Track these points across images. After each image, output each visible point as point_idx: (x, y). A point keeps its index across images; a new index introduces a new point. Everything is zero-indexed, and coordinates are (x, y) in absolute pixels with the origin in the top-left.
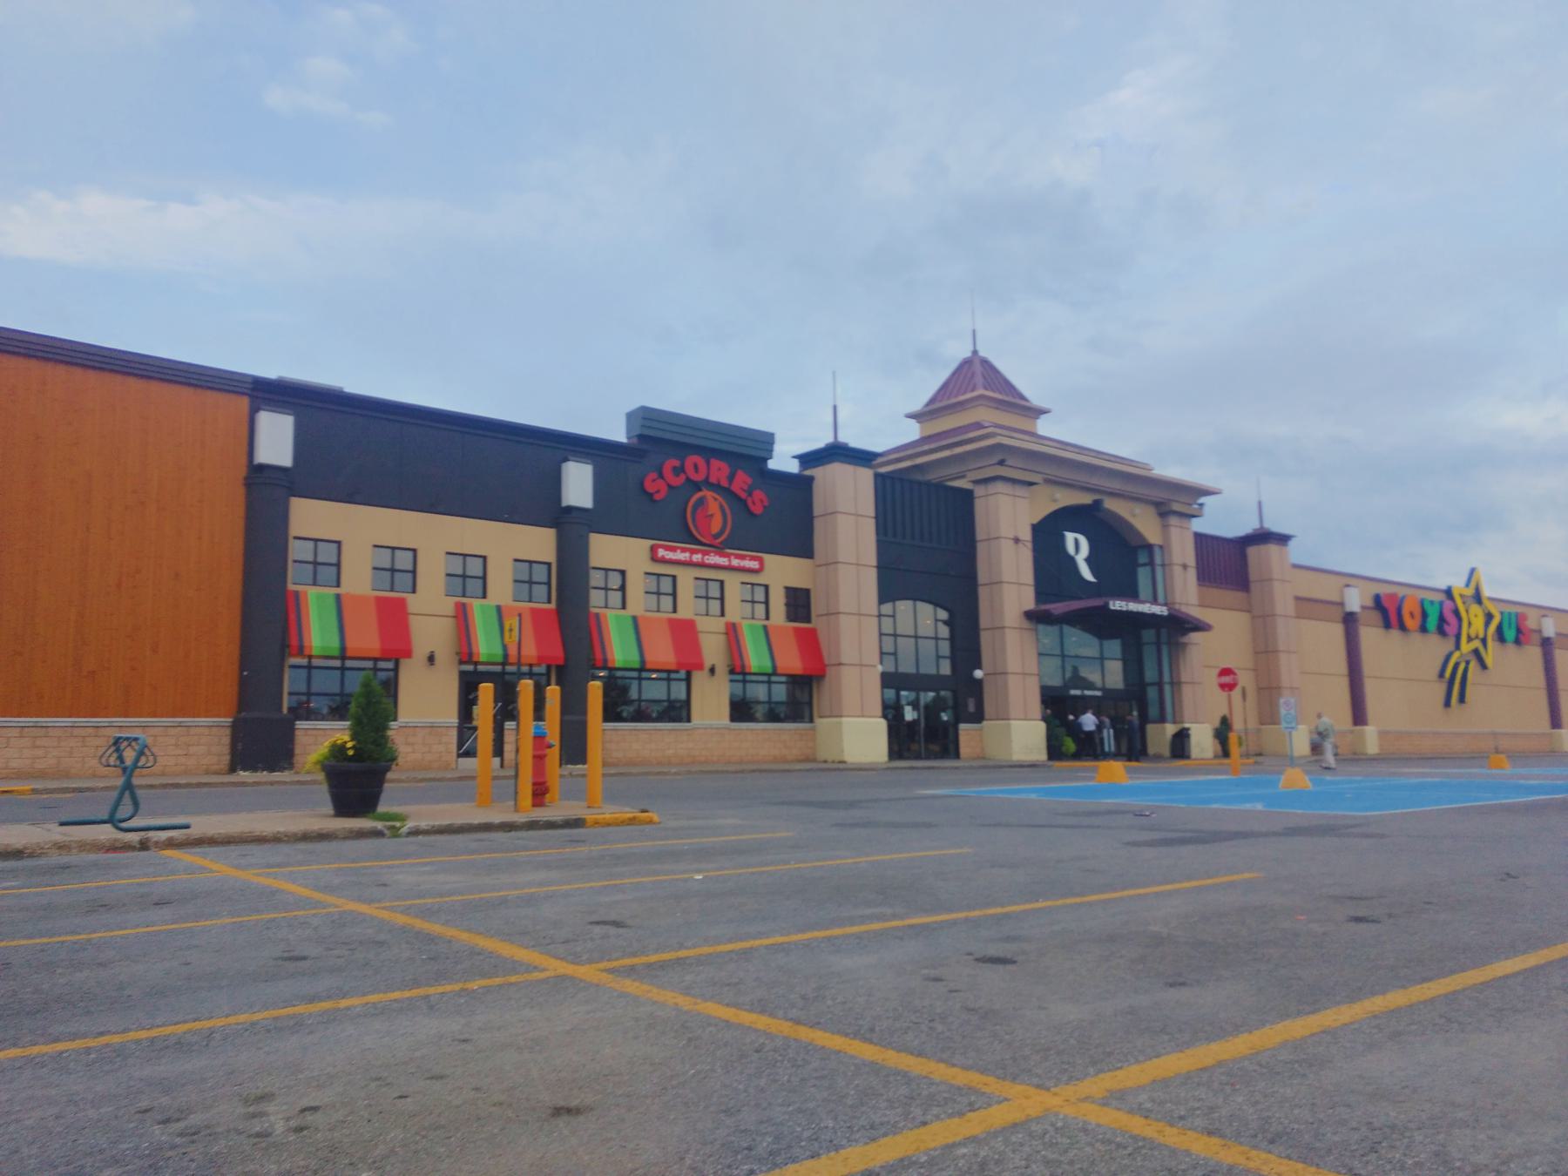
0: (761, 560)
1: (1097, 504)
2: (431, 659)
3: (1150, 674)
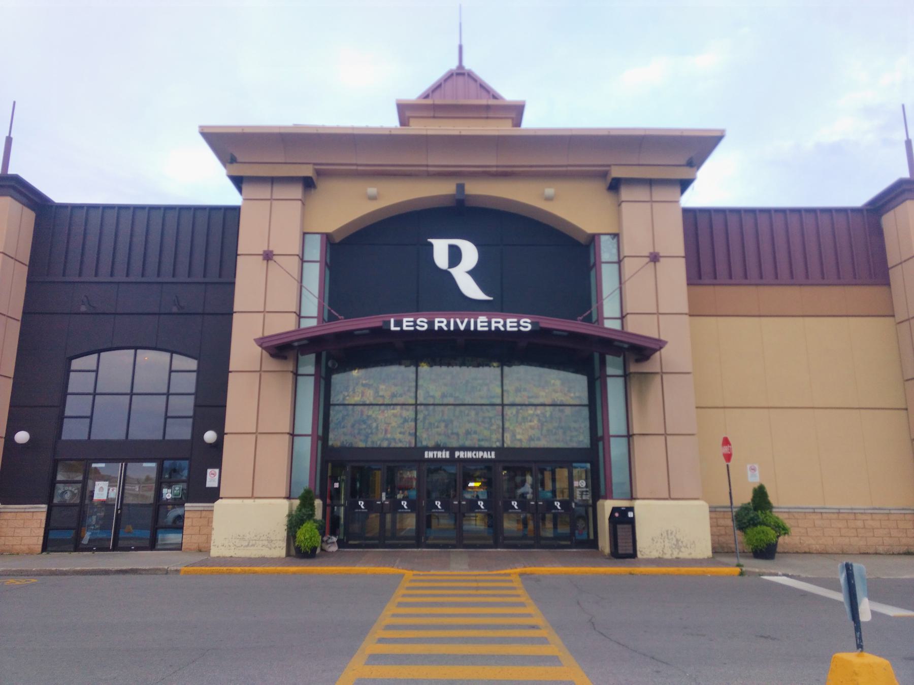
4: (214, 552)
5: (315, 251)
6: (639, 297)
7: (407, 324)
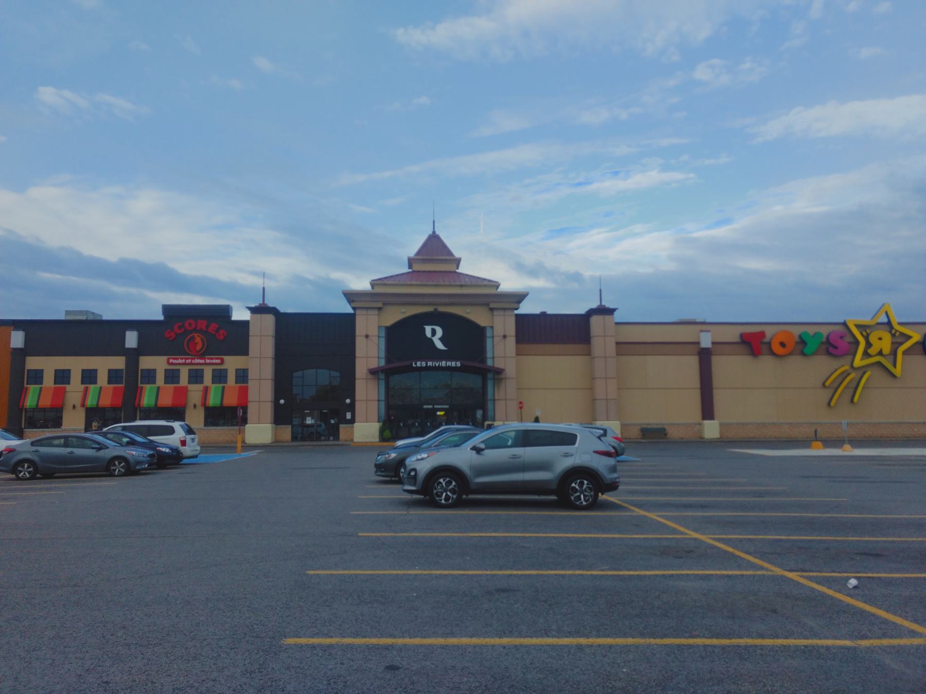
0: (222, 360)
1: (436, 309)
2: (74, 407)
3: (490, 396)
4: (355, 440)
5: (383, 334)
6: (499, 352)
7: (419, 364)
